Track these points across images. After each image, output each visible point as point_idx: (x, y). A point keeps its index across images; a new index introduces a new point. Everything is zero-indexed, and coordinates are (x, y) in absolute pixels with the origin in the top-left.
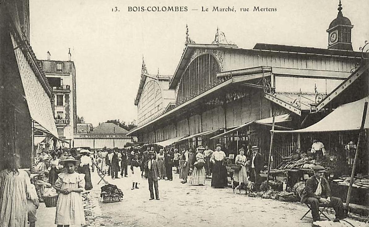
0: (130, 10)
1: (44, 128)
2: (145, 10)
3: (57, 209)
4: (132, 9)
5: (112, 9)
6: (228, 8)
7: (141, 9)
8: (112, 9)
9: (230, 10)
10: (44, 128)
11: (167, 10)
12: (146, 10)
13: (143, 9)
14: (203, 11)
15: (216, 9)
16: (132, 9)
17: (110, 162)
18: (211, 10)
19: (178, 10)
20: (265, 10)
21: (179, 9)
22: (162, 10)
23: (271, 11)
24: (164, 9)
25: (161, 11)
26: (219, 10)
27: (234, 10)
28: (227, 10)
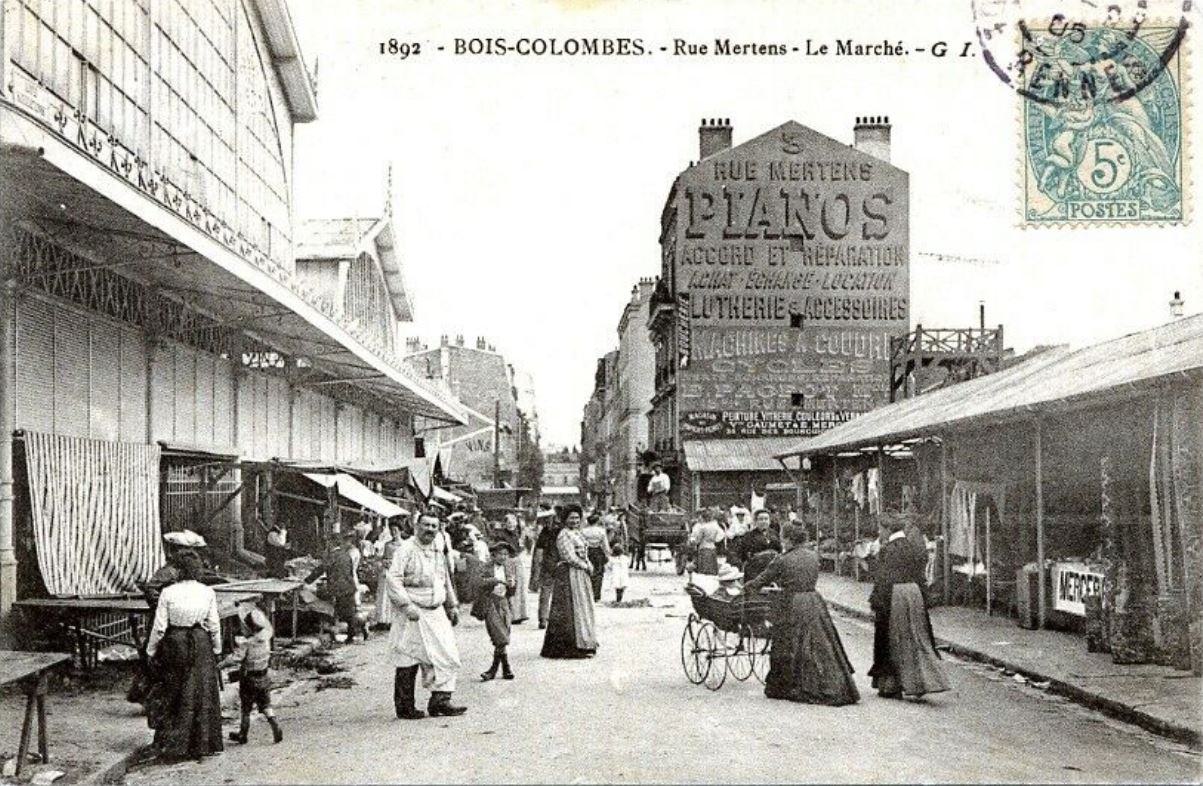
0: (461, 50)
1: (136, 72)
2: (507, 51)
3: (672, 575)
4: (467, 46)
5: (672, 606)
6: (883, 45)
7: (494, 47)
8: (672, 606)
9: (889, 50)
10: (136, 72)
11: (581, 50)
12: (512, 49)
13: (641, 48)
14: (808, 53)
15: (843, 48)
16: (467, 46)
17: (991, 510)
18: (833, 48)
19: (612, 50)
20: (749, 50)
21: (616, 47)
22: (564, 50)
23: (741, 55)
24: (572, 47)
25: (528, 52)
26: (853, 50)
27: (904, 51)
28: (878, 50)
